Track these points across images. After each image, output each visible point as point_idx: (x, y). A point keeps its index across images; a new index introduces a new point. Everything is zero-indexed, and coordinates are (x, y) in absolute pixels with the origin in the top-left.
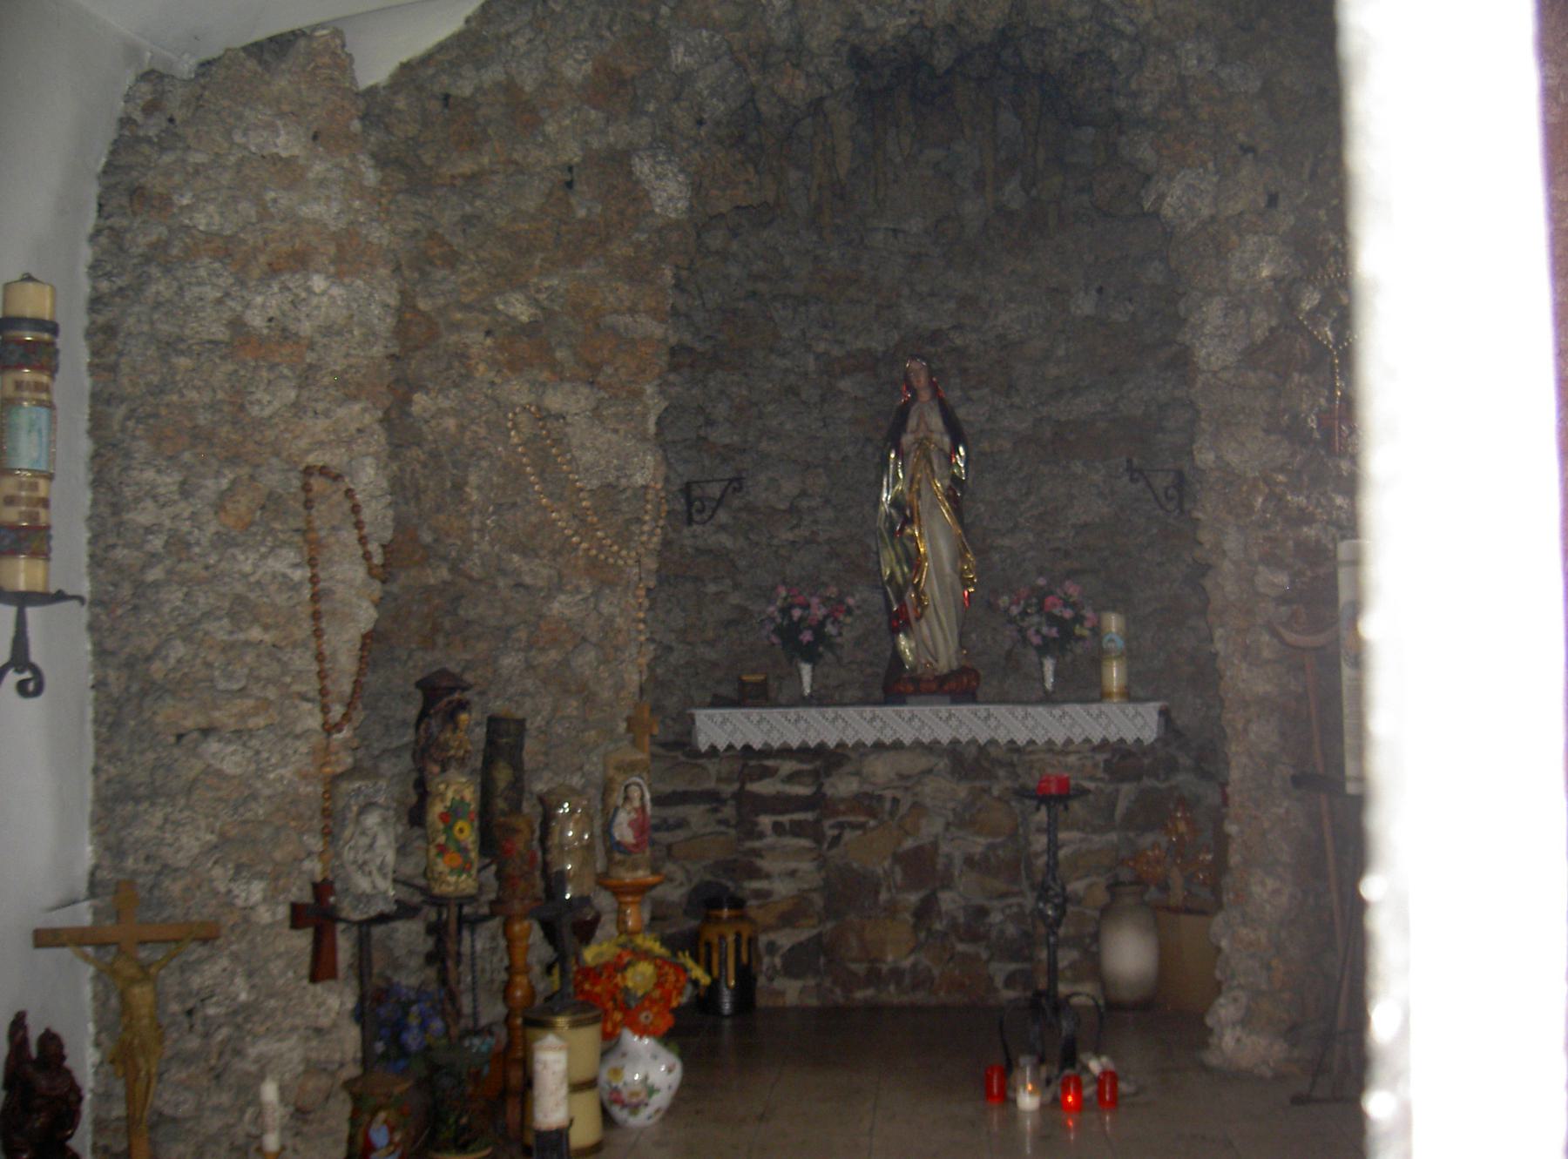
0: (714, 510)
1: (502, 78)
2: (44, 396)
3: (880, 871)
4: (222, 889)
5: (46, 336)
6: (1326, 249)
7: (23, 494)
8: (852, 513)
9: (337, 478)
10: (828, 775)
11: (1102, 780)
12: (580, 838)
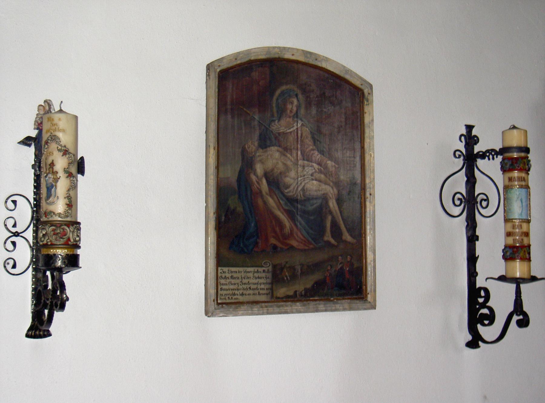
2: (523, 183)
5: (523, 154)
7: (517, 230)
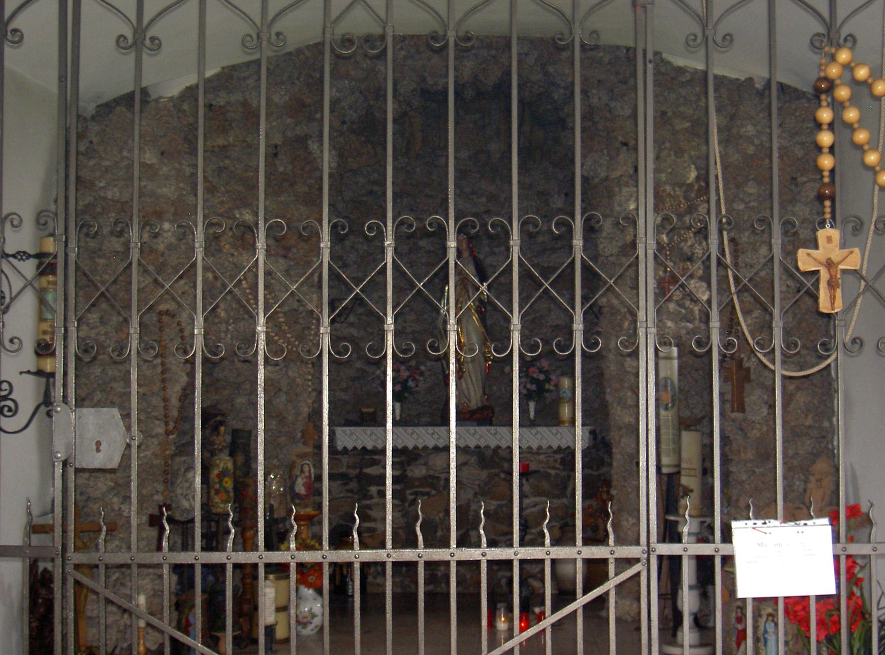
0: (348, 316)
1: (241, 99)
3: (437, 519)
4: (117, 508)
6: (664, 194)
8: (425, 316)
9: (173, 316)
10: (409, 465)
11: (558, 469)
12: (279, 490)
